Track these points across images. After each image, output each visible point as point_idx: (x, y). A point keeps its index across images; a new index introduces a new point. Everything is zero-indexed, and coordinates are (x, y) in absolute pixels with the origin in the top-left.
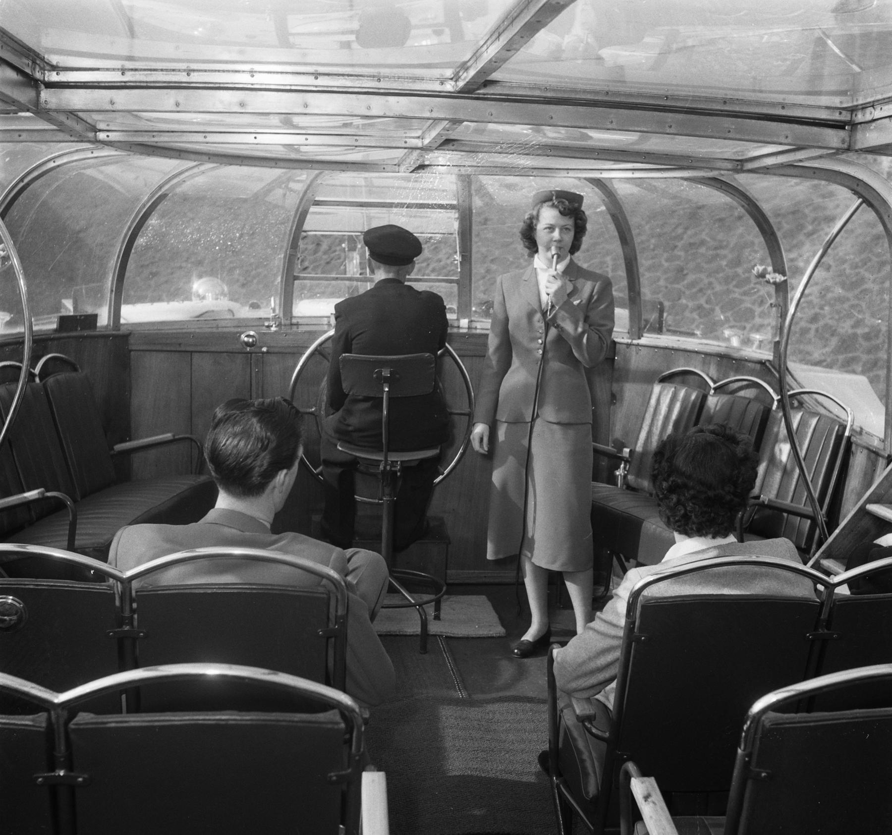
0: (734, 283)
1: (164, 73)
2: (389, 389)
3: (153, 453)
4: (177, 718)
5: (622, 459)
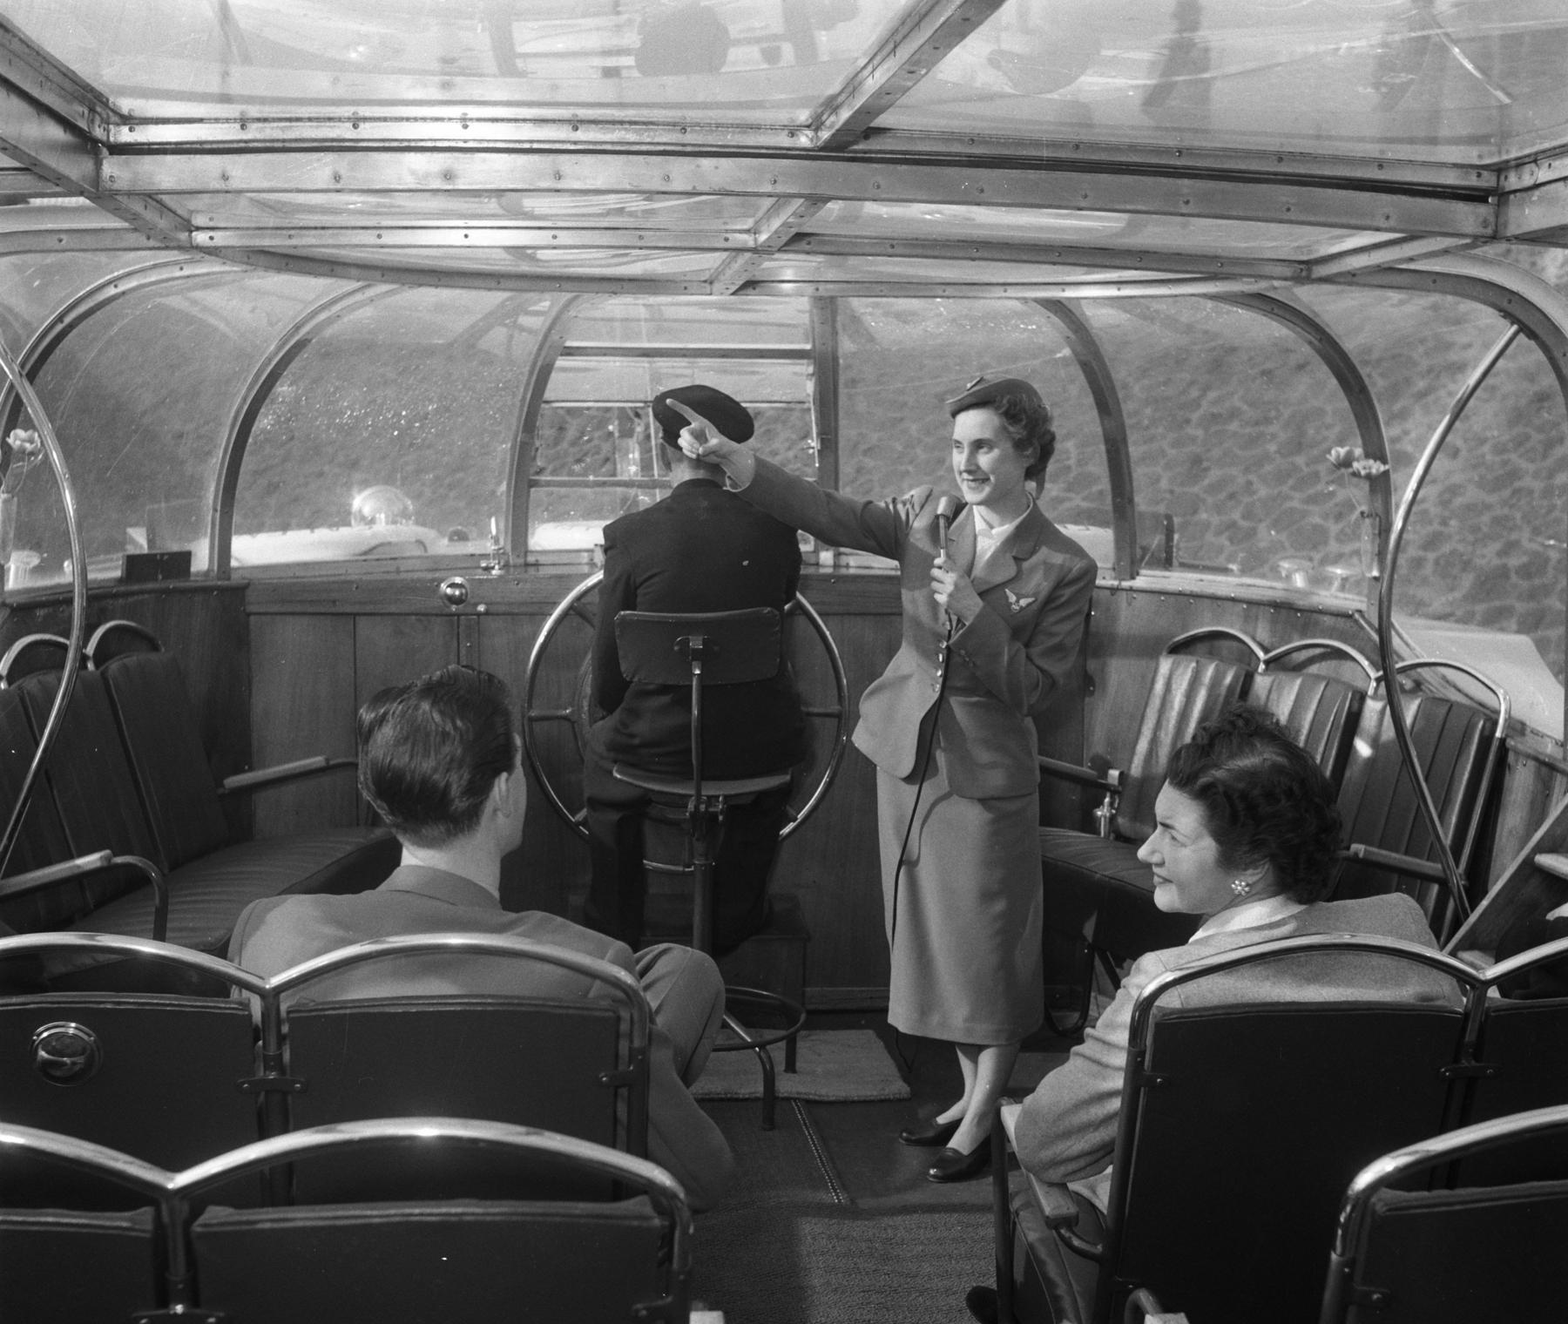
0: (1291, 482)
1: (315, 124)
2: (702, 671)
3: (290, 790)
4: (375, 1213)
5: (1106, 788)
